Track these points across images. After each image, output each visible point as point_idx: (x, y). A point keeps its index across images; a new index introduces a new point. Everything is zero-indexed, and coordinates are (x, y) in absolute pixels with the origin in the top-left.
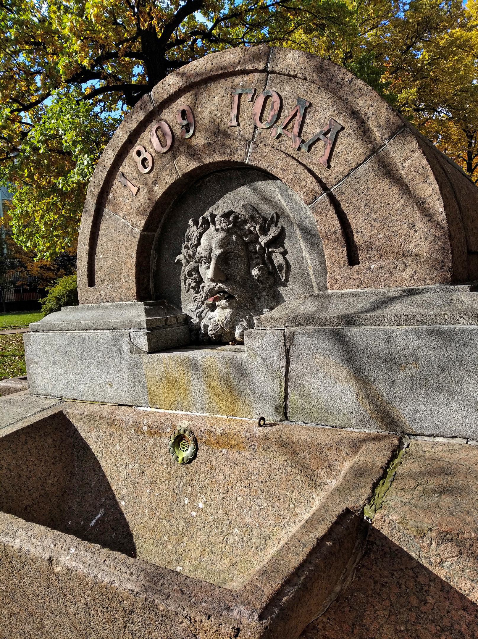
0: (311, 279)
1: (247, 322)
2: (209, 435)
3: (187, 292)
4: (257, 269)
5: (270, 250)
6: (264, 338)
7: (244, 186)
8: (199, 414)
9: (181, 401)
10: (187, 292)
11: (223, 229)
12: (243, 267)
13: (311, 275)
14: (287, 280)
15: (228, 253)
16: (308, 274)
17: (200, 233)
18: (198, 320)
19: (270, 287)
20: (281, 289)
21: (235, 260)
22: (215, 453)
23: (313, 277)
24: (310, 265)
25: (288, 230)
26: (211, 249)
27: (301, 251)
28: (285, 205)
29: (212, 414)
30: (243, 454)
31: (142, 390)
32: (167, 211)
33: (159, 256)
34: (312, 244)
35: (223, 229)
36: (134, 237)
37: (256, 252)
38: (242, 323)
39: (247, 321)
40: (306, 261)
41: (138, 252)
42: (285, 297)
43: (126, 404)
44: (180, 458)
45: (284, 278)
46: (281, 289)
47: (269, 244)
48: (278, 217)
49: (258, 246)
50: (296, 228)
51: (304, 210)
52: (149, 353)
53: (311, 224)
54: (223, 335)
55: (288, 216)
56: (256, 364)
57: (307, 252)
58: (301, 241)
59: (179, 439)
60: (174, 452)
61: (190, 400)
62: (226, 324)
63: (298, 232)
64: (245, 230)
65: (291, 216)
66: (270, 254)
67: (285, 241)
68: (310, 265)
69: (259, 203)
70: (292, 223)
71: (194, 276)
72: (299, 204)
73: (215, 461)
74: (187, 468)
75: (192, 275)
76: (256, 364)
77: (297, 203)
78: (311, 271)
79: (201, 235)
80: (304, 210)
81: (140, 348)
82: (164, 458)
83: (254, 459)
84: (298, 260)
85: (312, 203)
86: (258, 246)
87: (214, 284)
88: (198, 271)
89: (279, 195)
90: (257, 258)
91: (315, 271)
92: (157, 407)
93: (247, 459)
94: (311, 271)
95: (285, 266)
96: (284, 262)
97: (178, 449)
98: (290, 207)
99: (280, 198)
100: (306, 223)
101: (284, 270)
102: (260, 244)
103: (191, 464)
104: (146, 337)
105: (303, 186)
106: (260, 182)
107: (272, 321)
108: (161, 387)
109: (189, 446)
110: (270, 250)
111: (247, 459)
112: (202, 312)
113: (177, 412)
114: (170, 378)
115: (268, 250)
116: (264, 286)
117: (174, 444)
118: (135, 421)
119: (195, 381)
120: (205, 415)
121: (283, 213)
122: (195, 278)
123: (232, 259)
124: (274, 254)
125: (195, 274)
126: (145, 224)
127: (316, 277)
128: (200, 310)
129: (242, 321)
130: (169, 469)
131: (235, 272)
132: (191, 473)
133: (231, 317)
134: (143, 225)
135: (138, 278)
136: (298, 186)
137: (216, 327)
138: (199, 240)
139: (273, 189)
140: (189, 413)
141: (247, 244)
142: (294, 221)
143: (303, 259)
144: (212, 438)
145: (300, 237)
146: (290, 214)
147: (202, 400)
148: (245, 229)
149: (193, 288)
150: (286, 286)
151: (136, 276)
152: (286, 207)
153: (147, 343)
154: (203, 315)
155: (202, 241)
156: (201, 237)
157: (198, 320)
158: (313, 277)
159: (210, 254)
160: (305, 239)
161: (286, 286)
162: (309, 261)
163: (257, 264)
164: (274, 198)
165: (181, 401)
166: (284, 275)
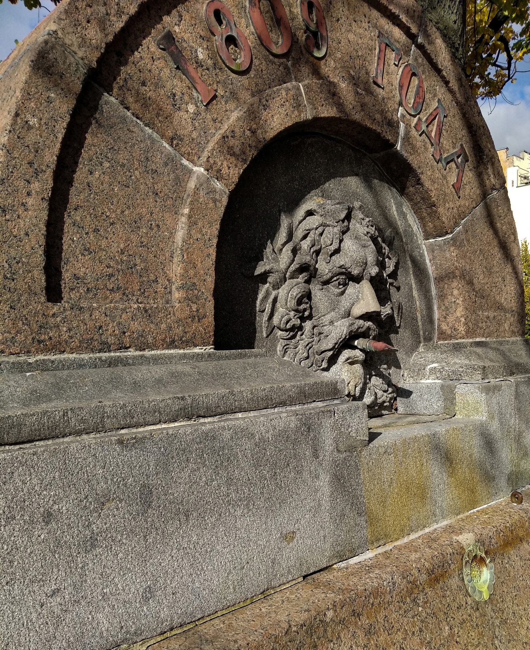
0: (419, 326)
3: (267, 337)
27: (411, 289)
28: (399, 223)
51: (415, 238)
63: (409, 262)
89: (394, 208)
99: (395, 213)
164: (389, 210)
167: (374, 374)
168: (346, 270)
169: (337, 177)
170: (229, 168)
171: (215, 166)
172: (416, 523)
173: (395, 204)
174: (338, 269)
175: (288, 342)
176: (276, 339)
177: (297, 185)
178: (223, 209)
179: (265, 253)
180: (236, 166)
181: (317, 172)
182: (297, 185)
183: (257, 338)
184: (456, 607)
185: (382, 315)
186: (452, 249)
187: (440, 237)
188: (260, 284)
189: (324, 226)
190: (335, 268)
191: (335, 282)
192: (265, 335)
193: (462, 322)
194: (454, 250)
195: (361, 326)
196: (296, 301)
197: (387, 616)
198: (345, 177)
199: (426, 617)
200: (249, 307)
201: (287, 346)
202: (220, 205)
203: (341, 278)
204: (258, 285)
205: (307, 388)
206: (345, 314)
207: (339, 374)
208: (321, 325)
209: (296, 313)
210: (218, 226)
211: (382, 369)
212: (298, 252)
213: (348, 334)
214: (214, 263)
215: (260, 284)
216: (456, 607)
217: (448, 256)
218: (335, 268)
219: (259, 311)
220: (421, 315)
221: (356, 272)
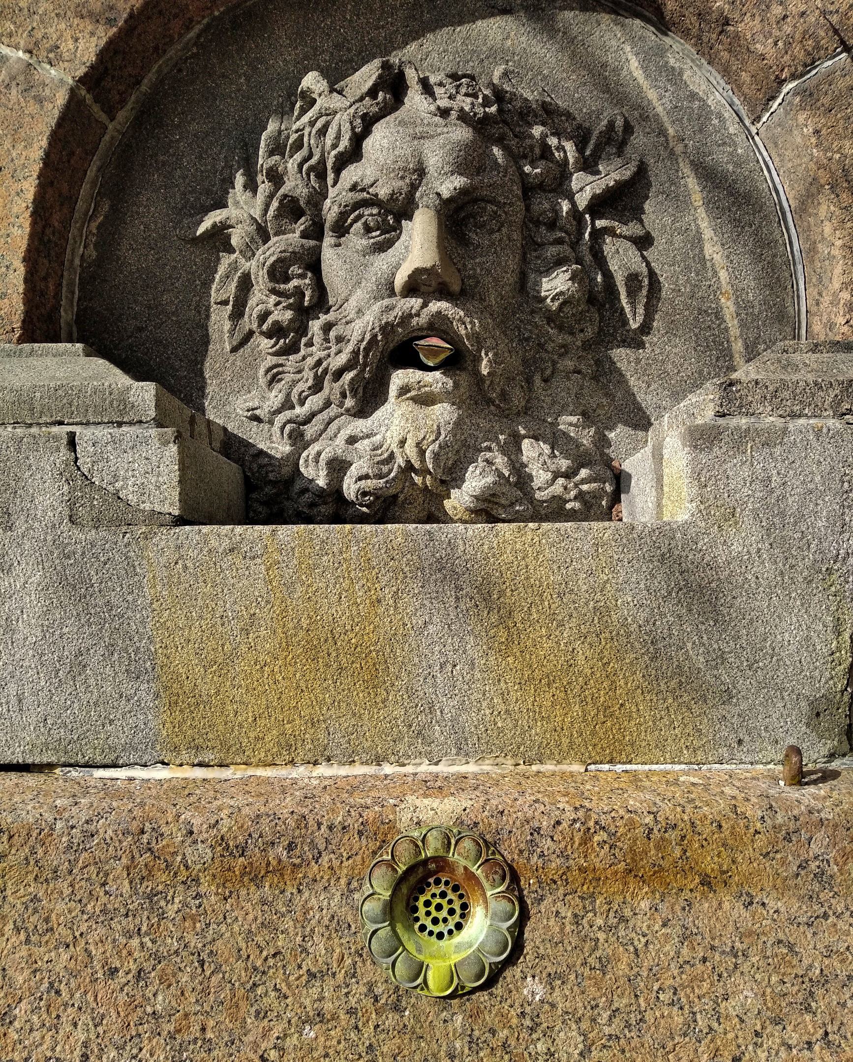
0: (727, 329)
1: (504, 453)
2: (584, 842)
3: (234, 350)
4: (568, 275)
5: (600, 223)
6: (778, 450)
7: (509, 18)
8: (443, 768)
9: (348, 722)
10: (234, 350)
11: (463, 117)
12: (512, 263)
13: (728, 318)
14: (646, 328)
15: (475, 201)
16: (718, 314)
17: (364, 117)
18: (288, 449)
19: (587, 346)
20: (621, 356)
21: (492, 231)
22: (623, 920)
23: (733, 325)
24: (725, 286)
25: (658, 173)
26: (421, 171)
27: (698, 240)
28: (652, 95)
29: (510, 762)
30: (772, 904)
31: (128, 688)
32: (171, 53)
33: (114, 209)
34: (736, 223)
35: (463, 117)
36: (39, 100)
37: (552, 225)
38: (489, 455)
39: (504, 451)
40: (715, 273)
41: (48, 160)
42: (632, 381)
43: (18, 758)
44: (436, 978)
45: (640, 319)
46: (621, 356)
47: (598, 207)
48: (628, 129)
49: (565, 206)
50: (686, 169)
51: (715, 122)
52: (180, 521)
53: (738, 165)
54: (402, 497)
55: (662, 132)
56: (736, 548)
57: (718, 248)
58: (701, 213)
59: (413, 880)
60: (395, 945)
61: (399, 712)
62: (436, 456)
63: (692, 183)
64: (528, 142)
65: (671, 132)
66: (597, 235)
67: (647, 206)
68: (725, 286)
69: (559, 76)
70: (672, 153)
71: (295, 282)
72: (700, 99)
73: (625, 958)
74: (475, 1015)
75: (287, 279)
76: (736, 548)
77: (693, 96)
78: (728, 306)
79: (369, 122)
80: (715, 122)
81: (133, 499)
82: (330, 983)
83: (825, 916)
84: (688, 268)
85: (802, 75)
86: (565, 206)
87: (415, 303)
88: (314, 266)
89: (634, 63)
90: (559, 242)
91: (743, 306)
92: (208, 757)
93: (792, 921)
94: (728, 306)
95: (646, 281)
96: (645, 271)
97: (409, 928)
98: (669, 106)
99: (639, 74)
100: (721, 158)
101: (644, 292)
102: (570, 197)
103: (498, 990)
104: (173, 449)
105: (773, 20)
106: (569, 15)
107: (786, 394)
108: (241, 666)
109: (464, 907)
110: (600, 223)
111: (792, 921)
112: (308, 420)
113: (323, 770)
114: (298, 626)
115: (593, 223)
116: (569, 339)
117: (389, 911)
118: (134, 826)
119: (431, 629)
120: (471, 768)
121: (644, 118)
122: (299, 293)
123: (482, 226)
124: (608, 240)
125: (302, 276)
126: (103, 55)
127: (743, 325)
128: (300, 411)
129: (489, 449)
130: (368, 1031)
131: (489, 271)
132: (503, 1034)
133: (454, 432)
134: (90, 57)
135: (31, 258)
136: (758, 19)
137: (385, 469)
138: (358, 140)
139: (614, 43)
140: (388, 769)
141: (529, 189)
142: (679, 149)
143: (704, 266)
144: (599, 858)
145: (697, 197)
146: (668, 125)
147: (462, 708)
148: (531, 136)
149: (277, 331)
150: (641, 345)
151: (29, 250)
152: (655, 103)
153: (175, 476)
154: (310, 431)
155: (368, 144)
156: (367, 131)
157: (288, 449)
158: (733, 325)
159: (414, 187)
160: (712, 206)
161: (641, 345)
162: (723, 275)
163: (560, 262)
164: (617, 71)
165: (348, 722)
166: (641, 310)
167: (523, 432)
168: (368, 193)
169: (442, 27)
170: (76, 40)
171: (45, 41)
172: (343, 741)
173: (637, 54)
174: (350, 194)
175: (281, 360)
176: (257, 356)
177: (325, 61)
178: (56, 113)
179: (230, 195)
180: (92, 34)
181: (383, 27)
182: (325, 61)
183: (211, 353)
184: (305, 968)
185: (547, 297)
186: (801, 118)
187: (773, 98)
188: (221, 254)
189: (327, 115)
190: (344, 193)
191: (355, 226)
192: (228, 348)
193: (842, 302)
194: (806, 120)
195: (413, 311)
196: (265, 271)
197: (40, 901)
198: (469, 22)
199: (176, 952)
200: (194, 296)
201: (281, 369)
202: (51, 106)
203: (366, 213)
204: (218, 255)
205: (38, 395)
206: (379, 290)
207: (386, 421)
208: (344, 321)
209: (278, 299)
210: (44, 143)
211: (564, 423)
212: (285, 179)
213: (377, 329)
214: (30, 205)
215: (221, 254)
216: (305, 968)
217: (799, 140)
218: (344, 193)
219: (215, 303)
220: (737, 303)
221: (382, 192)
